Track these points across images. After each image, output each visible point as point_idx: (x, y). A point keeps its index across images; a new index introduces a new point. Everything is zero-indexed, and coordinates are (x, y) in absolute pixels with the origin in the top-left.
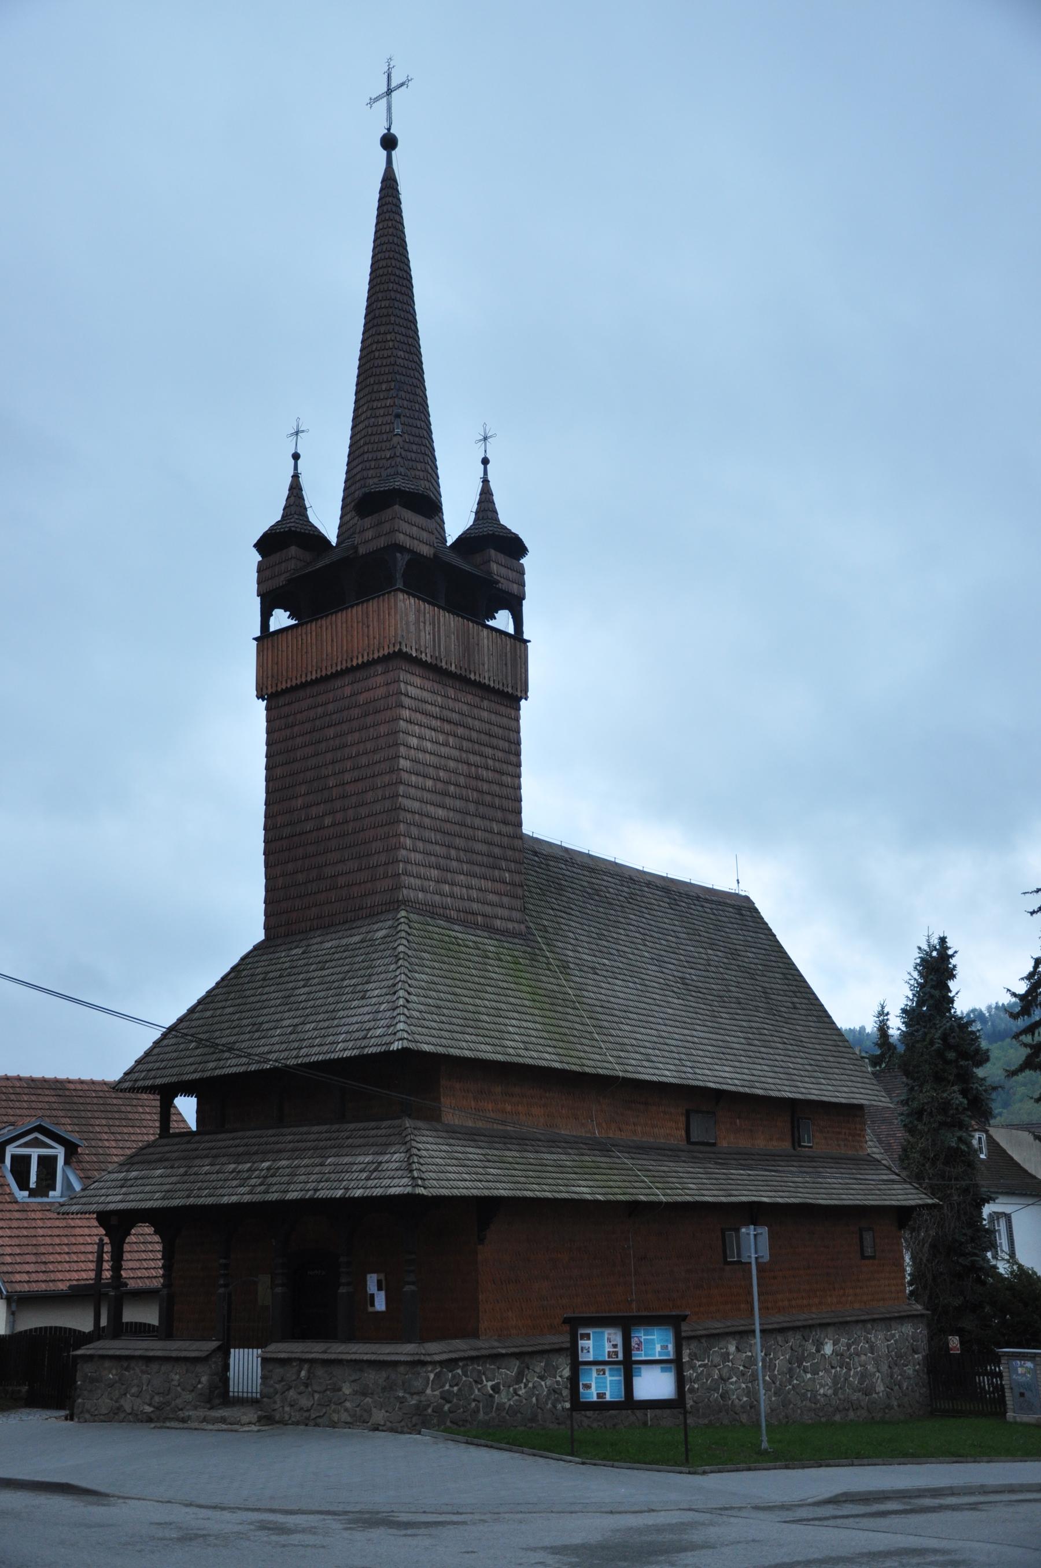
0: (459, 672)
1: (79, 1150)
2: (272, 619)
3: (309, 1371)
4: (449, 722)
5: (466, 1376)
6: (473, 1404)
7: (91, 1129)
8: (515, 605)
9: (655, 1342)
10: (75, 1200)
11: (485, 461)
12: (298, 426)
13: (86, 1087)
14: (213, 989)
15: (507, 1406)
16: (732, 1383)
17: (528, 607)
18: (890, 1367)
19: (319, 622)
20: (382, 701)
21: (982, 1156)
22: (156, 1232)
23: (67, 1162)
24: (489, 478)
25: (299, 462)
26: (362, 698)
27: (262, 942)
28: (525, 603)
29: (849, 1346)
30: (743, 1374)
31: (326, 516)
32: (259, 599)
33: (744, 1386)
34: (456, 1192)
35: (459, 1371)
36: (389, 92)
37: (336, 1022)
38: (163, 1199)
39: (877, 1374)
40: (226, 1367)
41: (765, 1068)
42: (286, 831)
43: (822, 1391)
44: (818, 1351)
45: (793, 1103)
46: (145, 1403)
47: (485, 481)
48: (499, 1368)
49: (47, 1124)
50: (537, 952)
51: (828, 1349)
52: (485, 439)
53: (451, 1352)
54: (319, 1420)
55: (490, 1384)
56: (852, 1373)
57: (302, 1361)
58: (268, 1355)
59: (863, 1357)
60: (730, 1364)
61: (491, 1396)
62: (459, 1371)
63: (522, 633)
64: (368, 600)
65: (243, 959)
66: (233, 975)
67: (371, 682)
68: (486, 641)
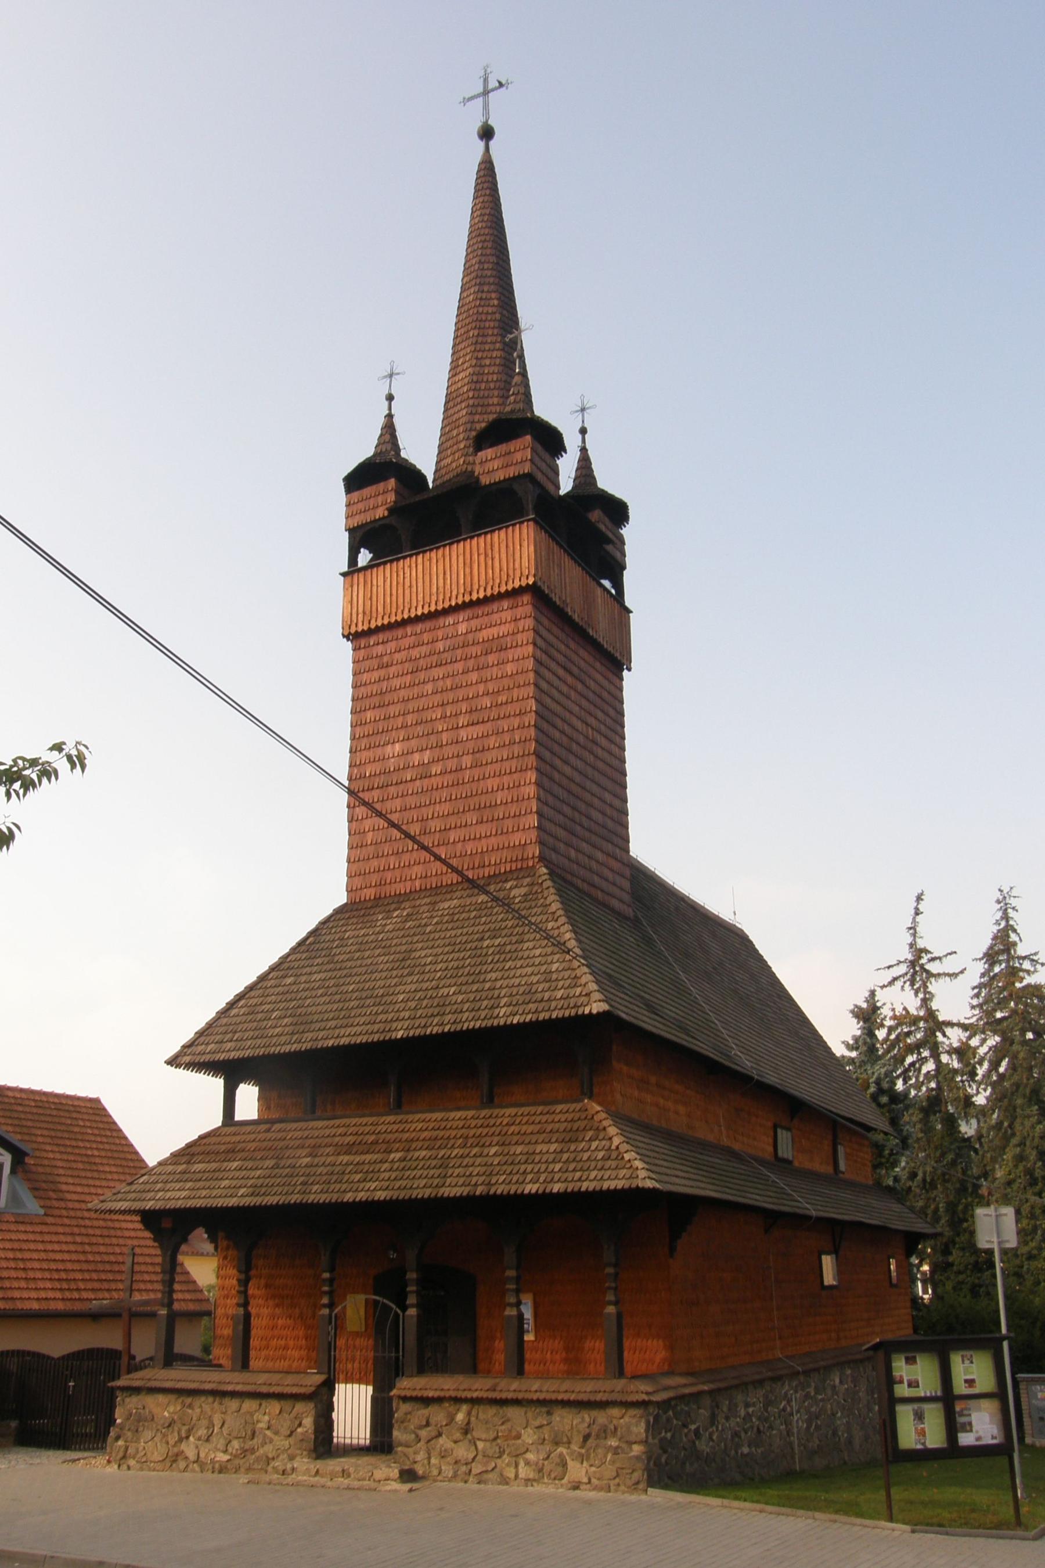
1: (27, 1160)
3: (469, 1414)
7: (34, 1138)
10: (120, 1196)
12: (392, 369)
13: (24, 1096)
14: (288, 955)
17: (627, 576)
22: (155, 1240)
23: (13, 1171)
26: (485, 634)
27: (345, 905)
28: (626, 573)
31: (422, 451)
32: (347, 534)
36: (486, 93)
40: (330, 1407)
54: (485, 1476)
57: (458, 1400)
64: (493, 531)
66: (311, 939)
67: (495, 617)
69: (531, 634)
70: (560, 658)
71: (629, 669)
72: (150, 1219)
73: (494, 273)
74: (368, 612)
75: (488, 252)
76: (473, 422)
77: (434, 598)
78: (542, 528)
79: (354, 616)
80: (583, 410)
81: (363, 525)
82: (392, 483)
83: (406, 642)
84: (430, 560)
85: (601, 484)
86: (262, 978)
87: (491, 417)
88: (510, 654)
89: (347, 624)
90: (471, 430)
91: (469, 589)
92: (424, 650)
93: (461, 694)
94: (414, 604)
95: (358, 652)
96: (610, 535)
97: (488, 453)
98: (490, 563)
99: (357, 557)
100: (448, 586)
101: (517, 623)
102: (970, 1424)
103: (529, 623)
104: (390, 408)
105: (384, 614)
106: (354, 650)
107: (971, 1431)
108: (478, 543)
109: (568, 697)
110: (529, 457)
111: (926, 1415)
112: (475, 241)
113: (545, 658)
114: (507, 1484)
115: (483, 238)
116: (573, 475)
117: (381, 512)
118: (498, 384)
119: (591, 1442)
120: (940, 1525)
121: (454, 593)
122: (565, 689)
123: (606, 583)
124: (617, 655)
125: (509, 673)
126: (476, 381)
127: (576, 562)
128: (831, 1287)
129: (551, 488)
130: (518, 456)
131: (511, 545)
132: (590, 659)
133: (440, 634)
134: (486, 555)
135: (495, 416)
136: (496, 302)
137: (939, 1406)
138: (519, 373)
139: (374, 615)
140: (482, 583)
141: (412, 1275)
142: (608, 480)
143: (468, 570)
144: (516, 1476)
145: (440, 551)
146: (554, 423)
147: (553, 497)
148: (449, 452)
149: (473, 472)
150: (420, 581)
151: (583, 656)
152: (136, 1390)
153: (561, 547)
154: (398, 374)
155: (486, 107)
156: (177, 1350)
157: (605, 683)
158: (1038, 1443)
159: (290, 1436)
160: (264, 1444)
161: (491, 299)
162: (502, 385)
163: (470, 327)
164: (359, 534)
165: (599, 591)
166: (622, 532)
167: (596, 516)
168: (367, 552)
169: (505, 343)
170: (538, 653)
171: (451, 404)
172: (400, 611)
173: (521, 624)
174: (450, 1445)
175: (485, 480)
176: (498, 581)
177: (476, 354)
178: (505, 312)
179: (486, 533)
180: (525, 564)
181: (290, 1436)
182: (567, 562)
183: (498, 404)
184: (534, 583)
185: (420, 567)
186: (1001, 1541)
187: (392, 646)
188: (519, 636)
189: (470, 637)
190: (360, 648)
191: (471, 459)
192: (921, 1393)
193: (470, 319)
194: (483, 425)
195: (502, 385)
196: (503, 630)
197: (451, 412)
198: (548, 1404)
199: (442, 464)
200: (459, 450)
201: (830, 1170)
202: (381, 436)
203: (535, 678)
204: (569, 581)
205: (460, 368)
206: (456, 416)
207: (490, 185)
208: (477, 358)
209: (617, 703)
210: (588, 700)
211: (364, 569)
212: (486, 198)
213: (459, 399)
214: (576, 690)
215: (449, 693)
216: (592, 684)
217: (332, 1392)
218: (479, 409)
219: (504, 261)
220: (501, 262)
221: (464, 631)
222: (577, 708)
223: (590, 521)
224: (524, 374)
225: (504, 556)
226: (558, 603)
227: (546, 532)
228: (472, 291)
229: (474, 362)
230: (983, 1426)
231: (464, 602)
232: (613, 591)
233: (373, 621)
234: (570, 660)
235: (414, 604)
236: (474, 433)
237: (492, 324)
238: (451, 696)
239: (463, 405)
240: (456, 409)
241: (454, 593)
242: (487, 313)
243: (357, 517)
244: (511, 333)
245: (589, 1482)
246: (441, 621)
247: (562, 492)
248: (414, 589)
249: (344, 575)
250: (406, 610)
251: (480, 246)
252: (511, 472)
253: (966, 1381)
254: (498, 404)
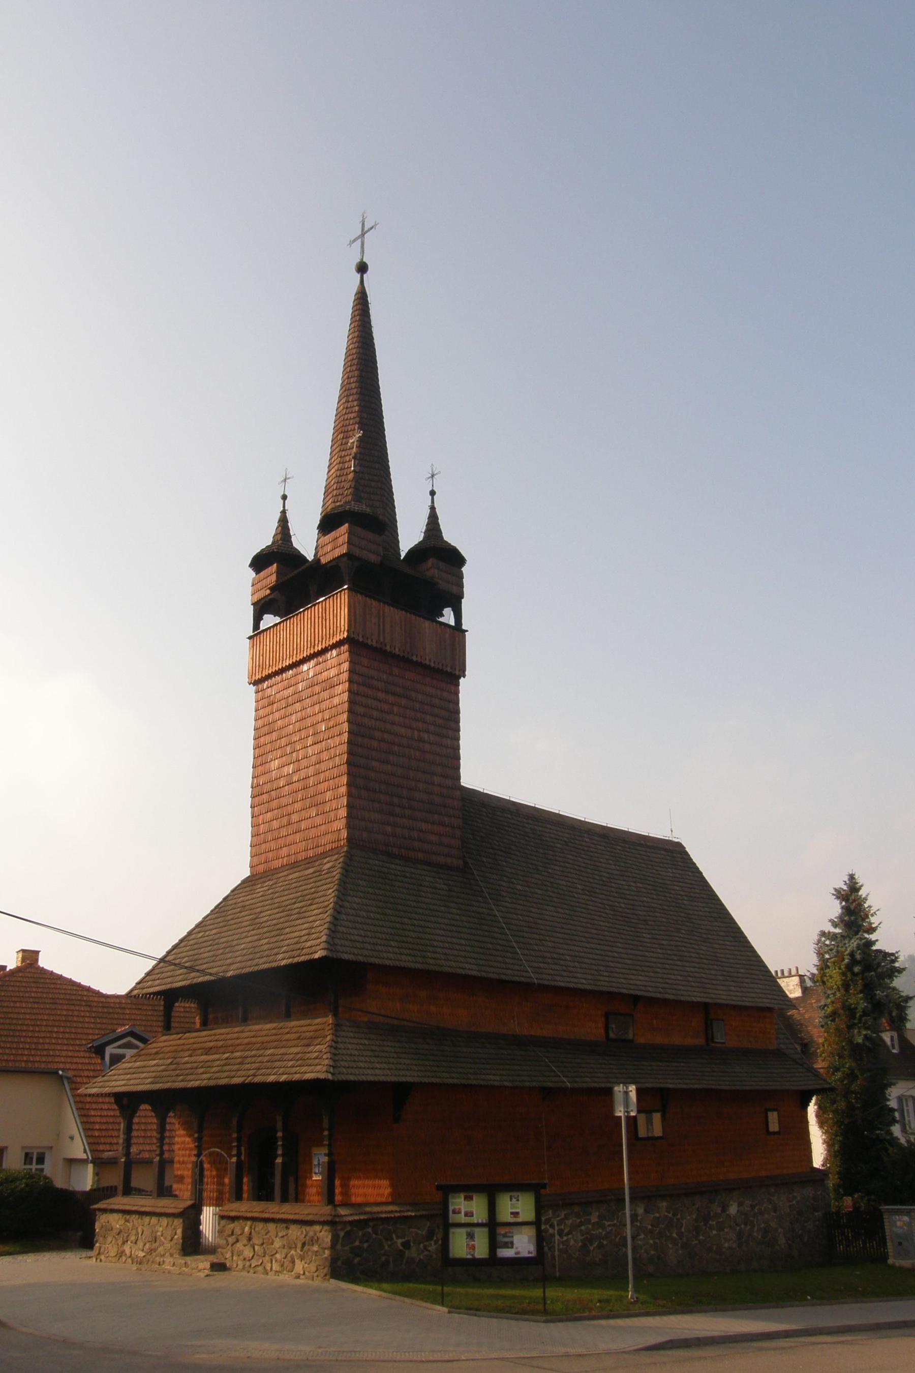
0: (402, 654)
3: (251, 1228)
4: (394, 694)
5: (377, 1234)
6: (383, 1258)
8: (456, 605)
9: (517, 1207)
11: (433, 493)
15: (417, 1260)
16: (640, 1240)
18: (791, 1223)
21: (894, 1051)
22: (152, 1110)
29: (753, 1207)
30: (651, 1232)
33: (651, 1242)
34: (364, 1078)
35: (370, 1230)
37: (282, 937)
38: (152, 1083)
39: (780, 1230)
41: (679, 978)
42: (267, 788)
43: (726, 1245)
44: (723, 1211)
45: (610, 993)
46: (139, 1249)
47: (433, 508)
48: (409, 1228)
49: (137, 1030)
50: (472, 882)
51: (733, 1210)
52: (433, 476)
53: (360, 1214)
55: (400, 1241)
56: (756, 1229)
58: (226, 1214)
59: (766, 1216)
60: (638, 1224)
61: (401, 1251)
62: (370, 1230)
63: (461, 625)
65: (233, 891)
72: (119, 1097)
86: (190, 933)
89: (251, 674)
102: (512, 1243)
107: (512, 1247)
111: (476, 1236)
114: (267, 1274)
119: (306, 1247)
120: (477, 1310)
128: (774, 1133)
137: (485, 1230)
141: (280, 1134)
144: (271, 1269)
152: (105, 1211)
156: (134, 1184)
158: (906, 1263)
159: (171, 1240)
160: (160, 1245)
174: (242, 1248)
181: (171, 1240)
186: (578, 1323)
192: (475, 1220)
198: (287, 1222)
201: (700, 1041)
217: (200, 1212)
230: (523, 1244)
245: (304, 1274)
253: (512, 1213)
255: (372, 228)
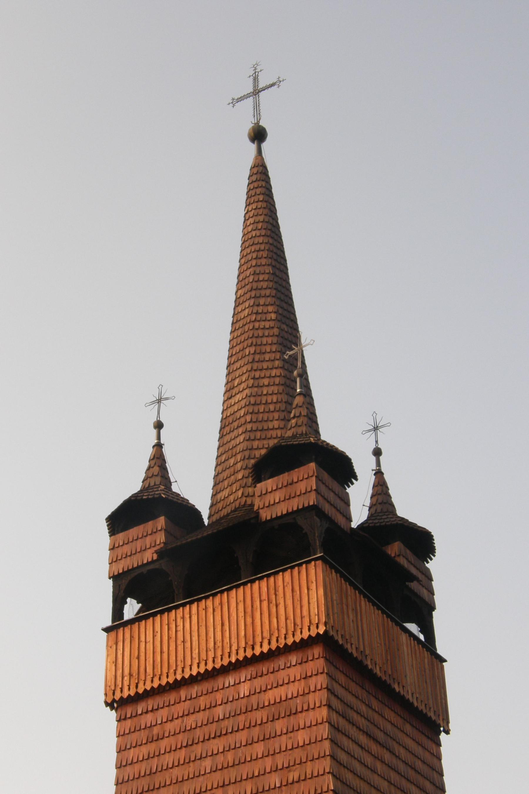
2: (126, 607)
12: (160, 393)
19: (203, 603)
20: (298, 701)
24: (383, 470)
25: (162, 431)
26: (271, 696)
31: (196, 485)
32: (111, 582)
36: (256, 92)
67: (282, 675)
68: (405, 648)
69: (324, 694)
70: (362, 722)
71: (447, 732)
73: (271, 284)
74: (135, 674)
75: (264, 261)
76: (252, 449)
77: (211, 654)
78: (332, 567)
79: (119, 679)
80: (376, 429)
81: (129, 571)
82: (161, 521)
83: (179, 709)
84: (206, 609)
85: (400, 513)
87: (272, 443)
88: (302, 719)
90: (249, 458)
91: (251, 643)
92: (201, 717)
93: (245, 770)
94: (188, 662)
95: (123, 722)
96: (414, 571)
97: (269, 484)
98: (274, 610)
99: (122, 609)
100: (227, 640)
101: (306, 681)
103: (322, 680)
104: (159, 437)
105: (154, 675)
106: (119, 721)
108: (260, 588)
109: (374, 771)
110: (314, 487)
112: (248, 250)
113: (342, 722)
115: (257, 247)
116: (368, 503)
117: (149, 556)
118: (278, 406)
121: (234, 647)
122: (369, 760)
123: (413, 627)
124: (431, 714)
125: (301, 744)
126: (254, 403)
127: (374, 604)
129: (340, 520)
130: (302, 487)
131: (297, 588)
132: (398, 721)
133: (219, 697)
134: (269, 602)
135: (276, 441)
136: (273, 316)
138: (300, 394)
139: (142, 677)
140: (266, 634)
142: (408, 507)
143: (249, 620)
145: (217, 599)
146: (341, 447)
147: (342, 530)
148: (226, 483)
149: (252, 505)
150: (195, 634)
151: (390, 718)
153: (356, 588)
154: (167, 399)
155: (257, 107)
157: (419, 751)
161: (268, 312)
162: (283, 406)
163: (245, 344)
164: (124, 582)
165: (404, 637)
166: (427, 565)
167: (395, 549)
168: (134, 601)
169: (284, 360)
170: (334, 716)
171: (227, 429)
172: (172, 671)
173: (312, 682)
175: (265, 515)
176: (283, 631)
177: (252, 374)
178: (284, 327)
179: (268, 576)
180: (314, 610)
182: (364, 605)
183: (279, 428)
184: (326, 632)
185: (195, 618)
187: (163, 713)
188: (311, 696)
189: (254, 699)
190: (125, 719)
191: (250, 490)
193: (246, 336)
194: (263, 452)
195: (283, 406)
196: (293, 689)
197: (227, 438)
199: (219, 496)
200: (236, 481)
202: (148, 469)
203: (332, 748)
204: (368, 628)
205: (236, 390)
206: (233, 443)
207: (263, 190)
208: (254, 378)
209: (435, 775)
210: (399, 774)
211: (131, 622)
212: (260, 205)
213: (235, 424)
214: (383, 762)
215: (231, 769)
216: (402, 752)
218: (258, 434)
219: (279, 243)
220: (278, 273)
221: (247, 693)
222: (386, 783)
223: (388, 557)
224: (307, 393)
225: (289, 602)
226: (355, 655)
227: (337, 571)
228: (247, 304)
229: (251, 382)
231: (246, 657)
232: (422, 637)
233: (141, 685)
234: (373, 723)
235: (188, 662)
236: (253, 461)
237: (270, 340)
238: (232, 774)
239: (240, 430)
240: (232, 435)
241: (234, 647)
242: (264, 328)
243: (123, 561)
244: (291, 349)
246: (220, 682)
247: (354, 525)
248: (188, 645)
249: (107, 630)
250: (179, 671)
251: (254, 255)
252: (295, 504)
254: (279, 428)
255: (272, 85)
